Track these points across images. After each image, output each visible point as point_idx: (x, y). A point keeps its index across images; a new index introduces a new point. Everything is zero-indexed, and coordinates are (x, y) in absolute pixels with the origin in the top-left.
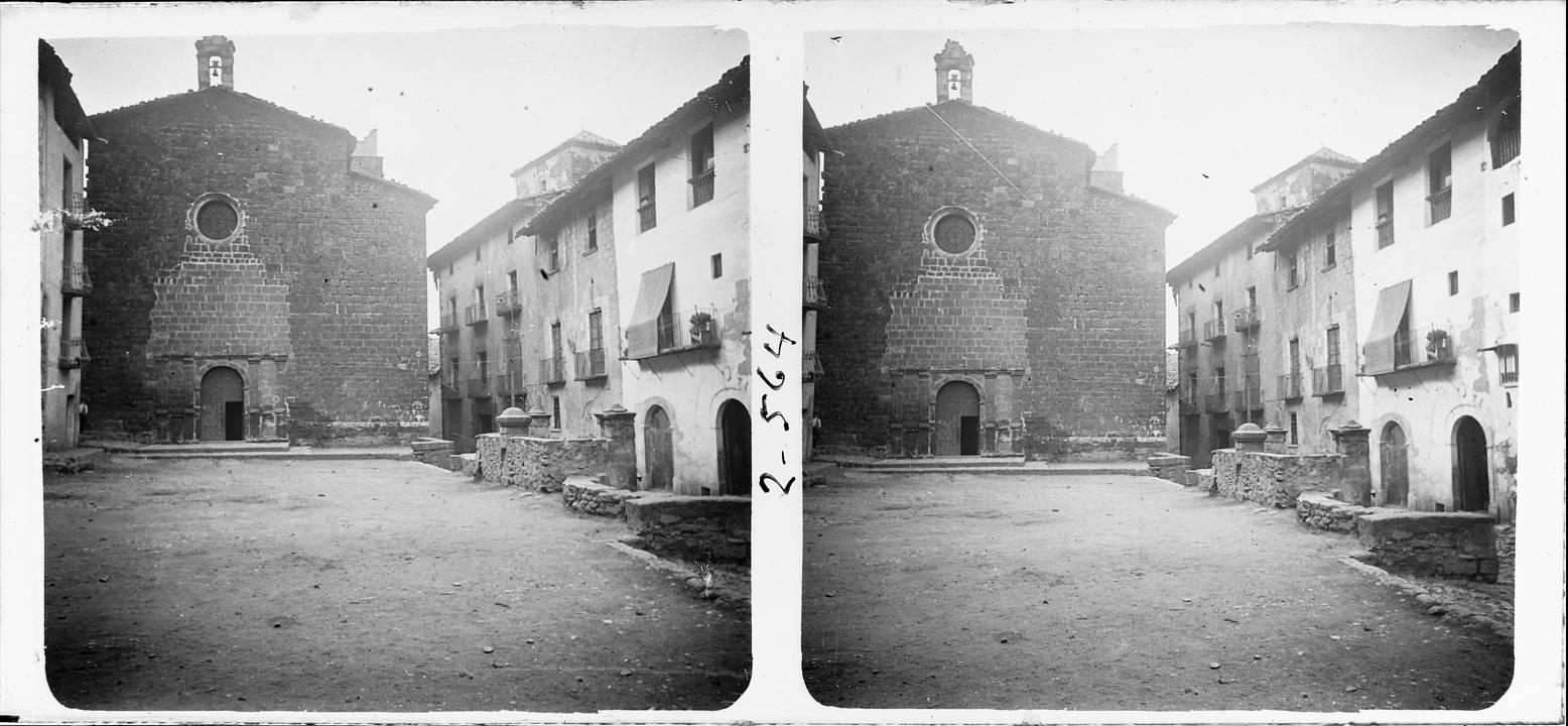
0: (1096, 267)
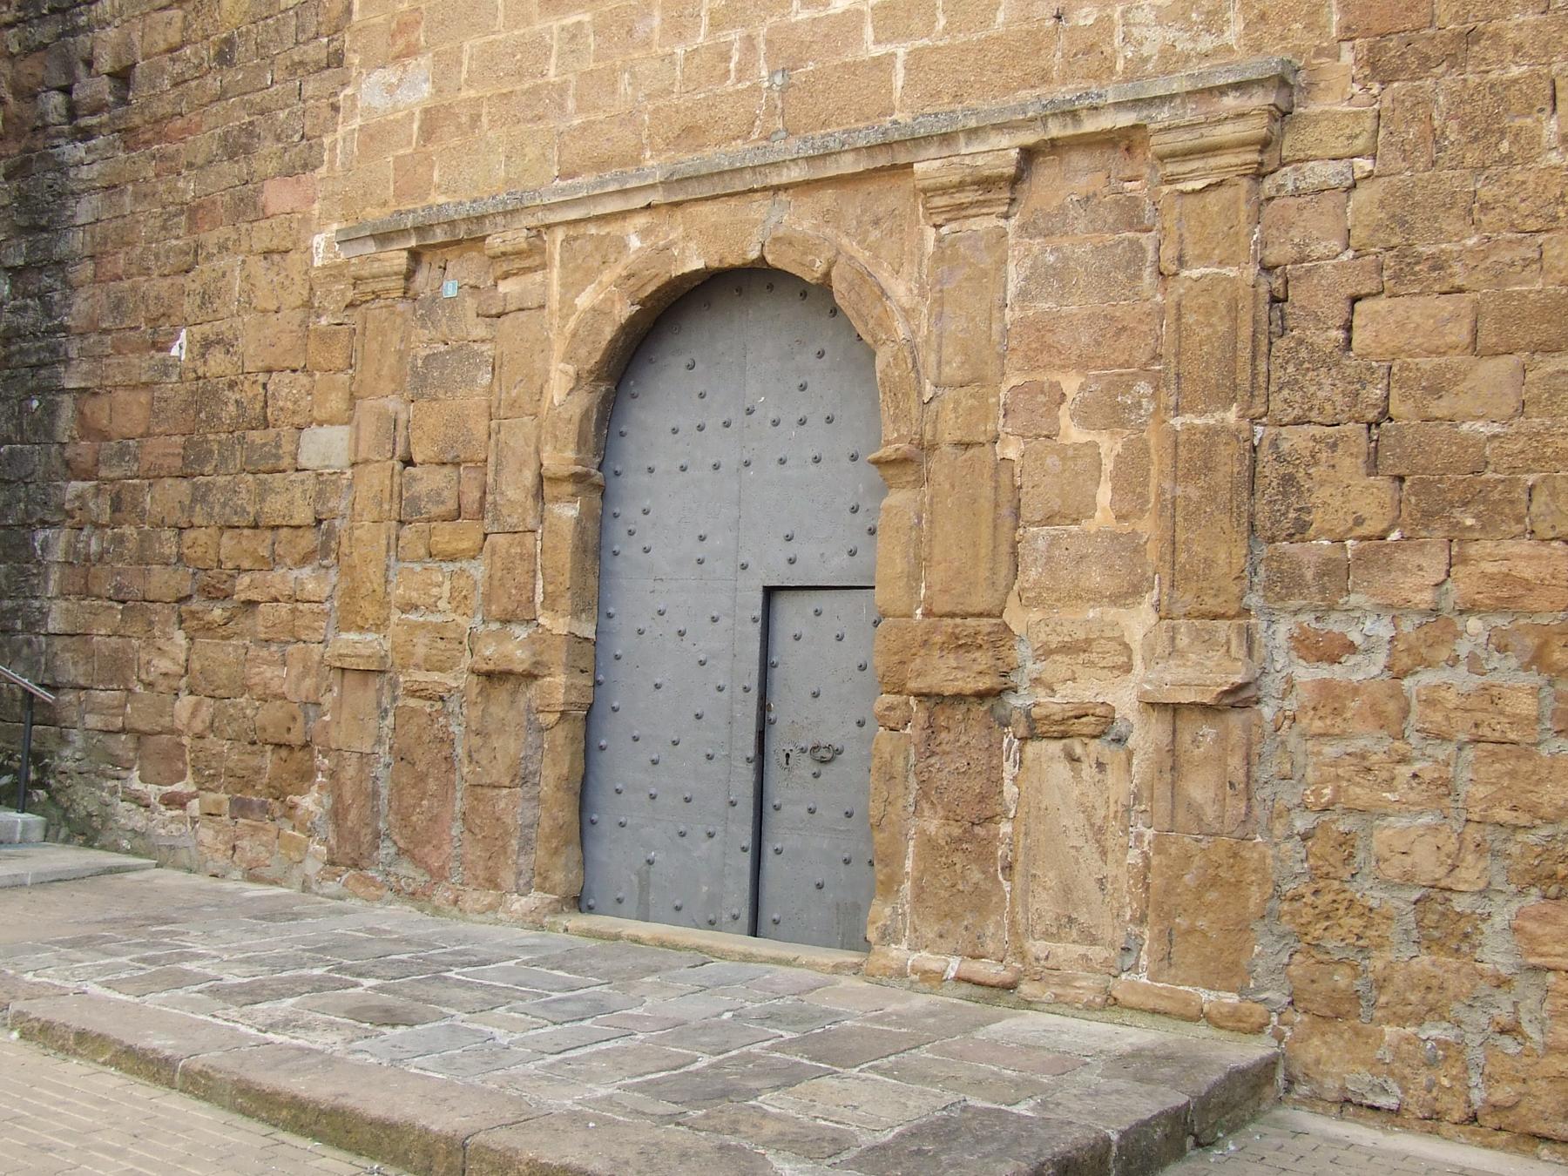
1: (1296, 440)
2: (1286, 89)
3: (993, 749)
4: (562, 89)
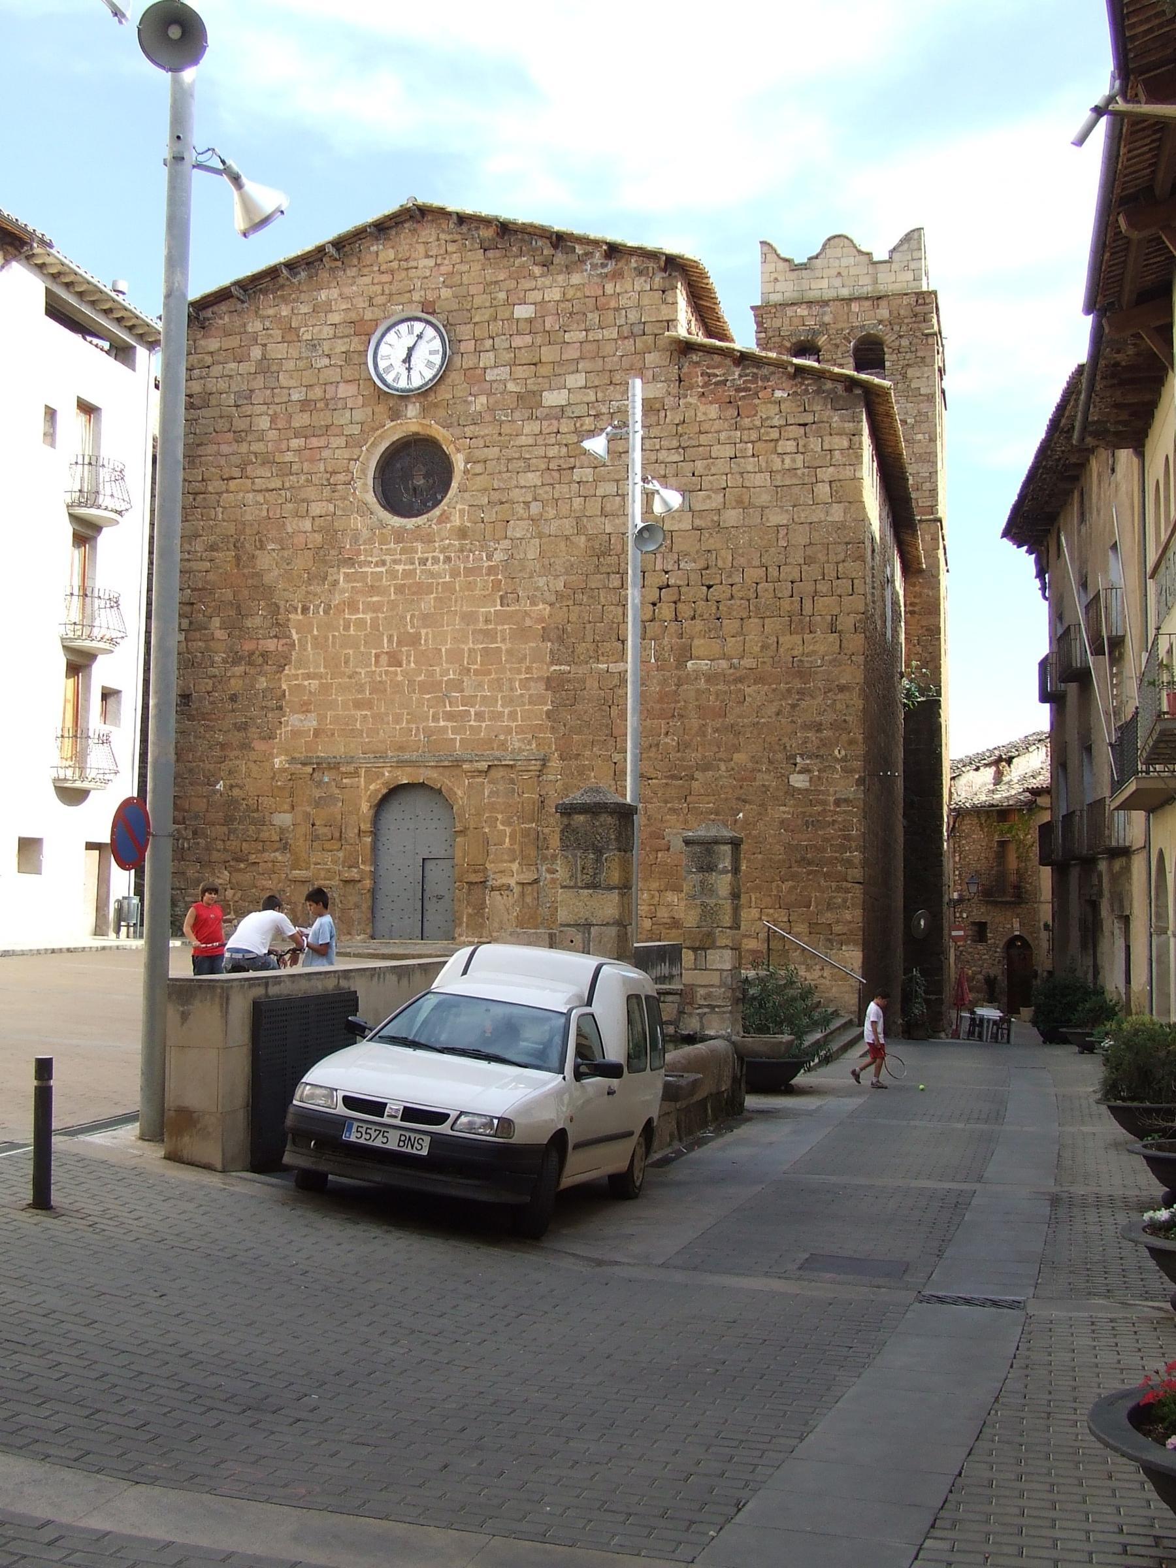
0: (698, 522)
1: (546, 830)
2: (544, 761)
3: (484, 893)
4: (362, 731)
